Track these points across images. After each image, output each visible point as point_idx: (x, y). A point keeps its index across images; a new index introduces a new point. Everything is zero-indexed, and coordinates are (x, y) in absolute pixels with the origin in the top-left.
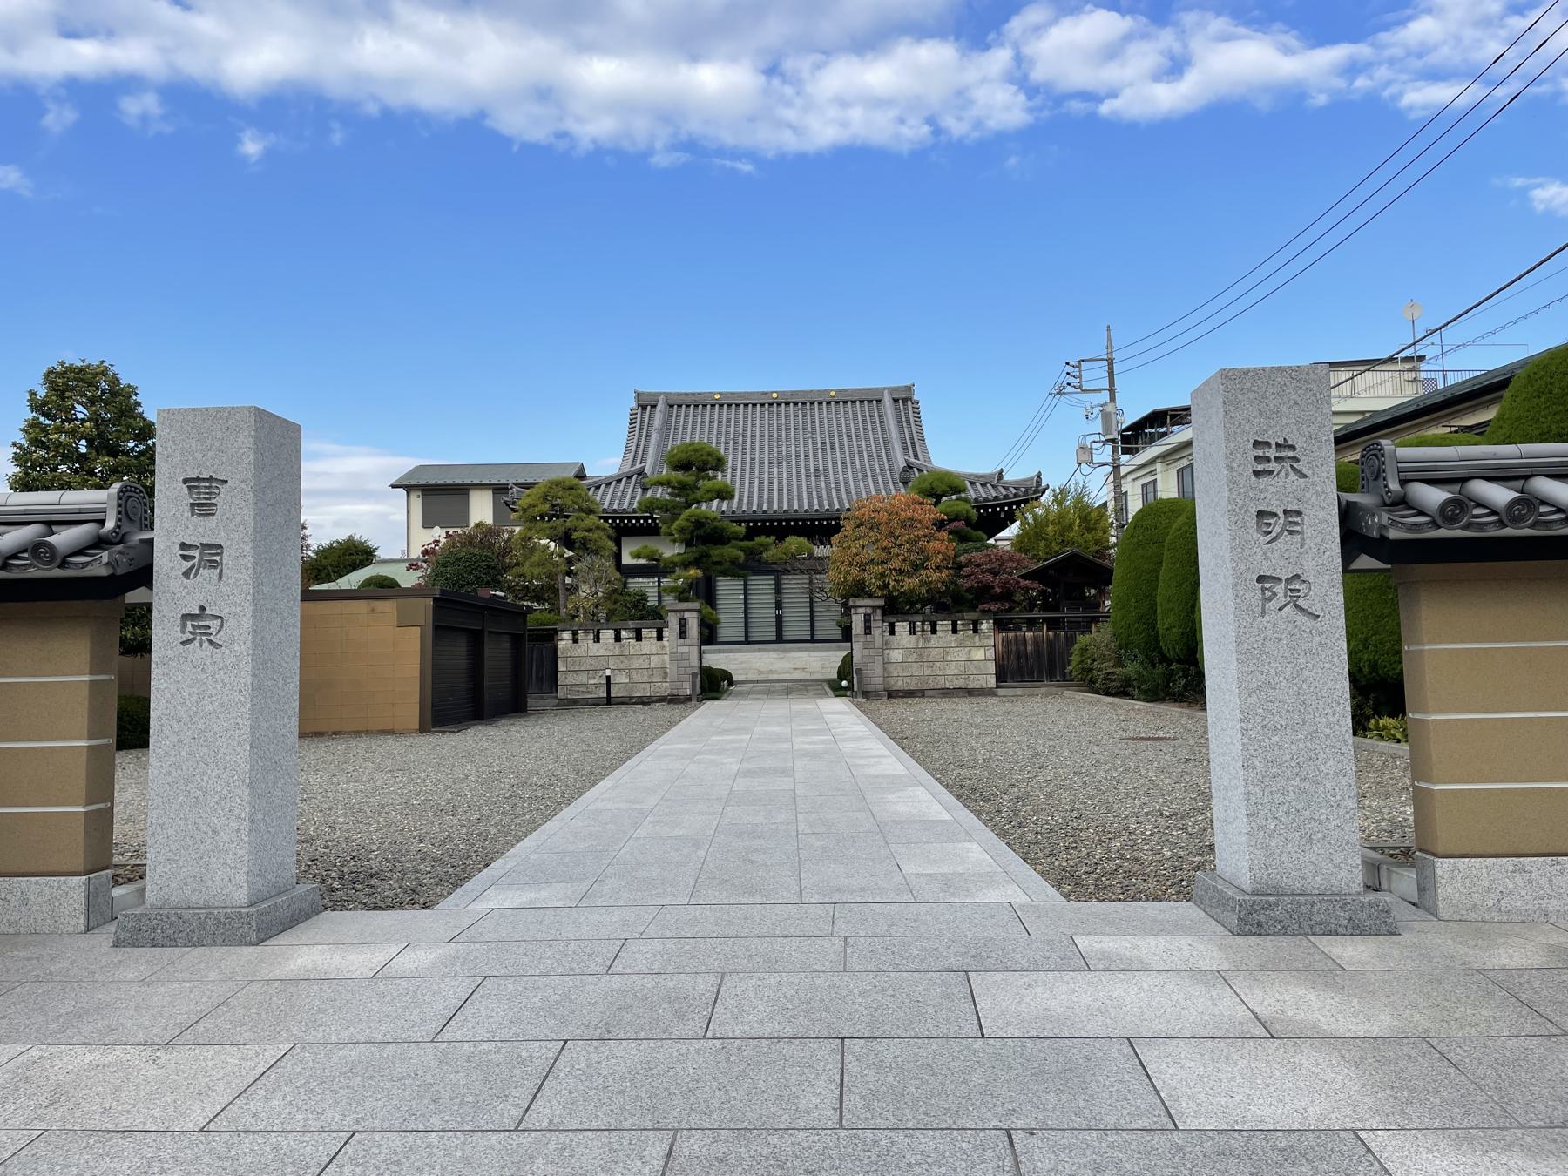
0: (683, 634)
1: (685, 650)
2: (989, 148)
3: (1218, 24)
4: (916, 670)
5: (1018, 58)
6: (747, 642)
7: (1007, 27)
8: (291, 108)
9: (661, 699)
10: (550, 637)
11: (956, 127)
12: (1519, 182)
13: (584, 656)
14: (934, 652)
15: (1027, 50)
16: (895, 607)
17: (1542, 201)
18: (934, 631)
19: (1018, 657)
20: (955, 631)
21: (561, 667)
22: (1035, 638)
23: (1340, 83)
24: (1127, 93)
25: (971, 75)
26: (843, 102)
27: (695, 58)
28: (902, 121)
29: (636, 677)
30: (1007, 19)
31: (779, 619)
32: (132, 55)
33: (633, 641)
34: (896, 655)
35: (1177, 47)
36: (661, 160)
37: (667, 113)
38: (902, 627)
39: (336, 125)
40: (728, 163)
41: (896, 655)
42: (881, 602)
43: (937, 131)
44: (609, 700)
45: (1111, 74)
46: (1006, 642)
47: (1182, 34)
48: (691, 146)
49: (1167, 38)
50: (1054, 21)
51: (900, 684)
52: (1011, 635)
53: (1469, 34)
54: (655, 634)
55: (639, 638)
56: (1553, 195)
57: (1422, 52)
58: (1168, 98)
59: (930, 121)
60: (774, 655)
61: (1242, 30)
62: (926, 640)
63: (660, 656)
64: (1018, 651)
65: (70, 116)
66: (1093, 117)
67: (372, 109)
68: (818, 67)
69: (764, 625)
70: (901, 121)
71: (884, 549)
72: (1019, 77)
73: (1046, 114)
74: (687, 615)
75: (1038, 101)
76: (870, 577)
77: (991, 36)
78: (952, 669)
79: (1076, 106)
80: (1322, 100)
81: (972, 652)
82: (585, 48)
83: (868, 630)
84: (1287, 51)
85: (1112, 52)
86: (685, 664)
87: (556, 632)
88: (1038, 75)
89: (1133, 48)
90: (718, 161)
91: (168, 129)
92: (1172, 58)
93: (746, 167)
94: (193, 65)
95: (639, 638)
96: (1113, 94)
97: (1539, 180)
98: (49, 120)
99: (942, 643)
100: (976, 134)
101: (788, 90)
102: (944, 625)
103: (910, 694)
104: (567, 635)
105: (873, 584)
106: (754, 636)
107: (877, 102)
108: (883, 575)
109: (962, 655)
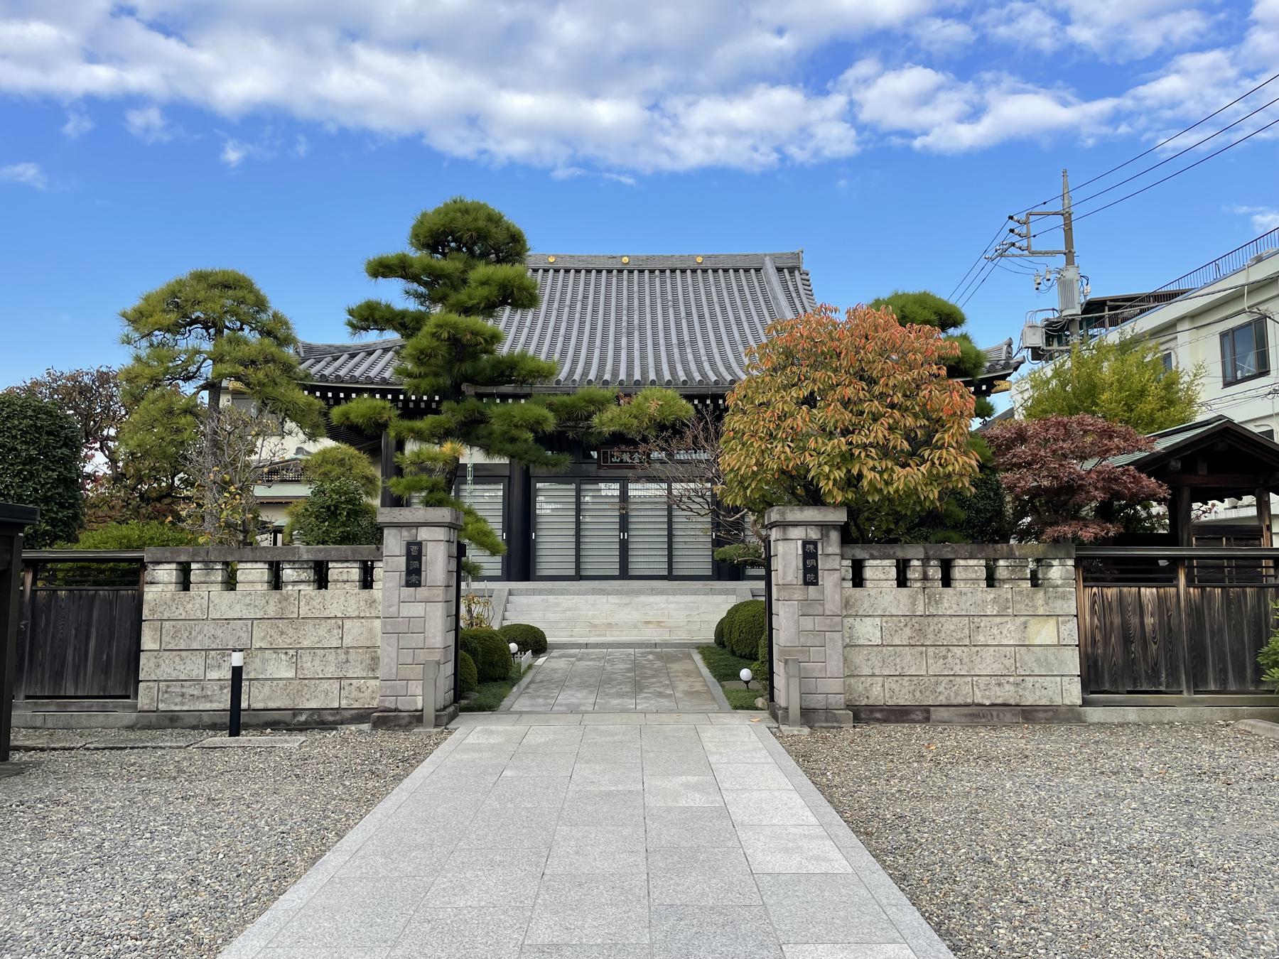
0: (413, 575)
1: (416, 610)
2: (828, 170)
3: (1009, 81)
4: (911, 663)
5: (852, 103)
6: (579, 577)
7: (842, 77)
8: (261, 122)
9: (361, 716)
10: (131, 575)
11: (798, 154)
12: (1244, 209)
13: (195, 624)
14: (949, 625)
15: (856, 96)
16: (875, 529)
17: (1261, 225)
18: (947, 581)
19: (1127, 640)
20: (991, 581)
21: (148, 641)
22: (1161, 600)
23: (1105, 130)
24: (936, 131)
25: (815, 115)
26: (710, 132)
27: (594, 95)
28: (755, 149)
29: (311, 666)
30: (842, 72)
31: (624, 547)
32: (140, 78)
33: (308, 589)
34: (868, 630)
35: (976, 99)
36: (561, 174)
37: (569, 137)
38: (880, 571)
39: (301, 138)
40: (615, 177)
41: (868, 630)
42: (841, 516)
43: (784, 157)
44: (235, 722)
45: (925, 116)
46: (1101, 608)
47: (981, 87)
48: (586, 164)
49: (968, 90)
50: (880, 75)
51: (878, 693)
52: (1111, 592)
53: (1210, 93)
54: (355, 573)
55: (322, 581)
56: (1268, 220)
57: (1174, 104)
58: (968, 135)
59: (778, 150)
60: (614, 599)
61: (1030, 86)
62: (932, 600)
63: (365, 628)
64: (1125, 626)
65: (87, 125)
66: (908, 150)
67: (332, 128)
68: (689, 105)
69: (602, 556)
70: (755, 149)
71: (846, 403)
72: (850, 115)
73: (871, 146)
74: (423, 534)
75: (867, 134)
76: (819, 463)
77: (830, 84)
78: (988, 663)
79: (896, 141)
80: (1091, 142)
81: (1023, 625)
82: (503, 85)
83: (810, 575)
84: (1065, 104)
85: (925, 99)
86: (416, 641)
87: (142, 565)
88: (865, 116)
89: (942, 97)
90: (607, 175)
91: (167, 138)
92: (974, 107)
93: (629, 181)
94: (188, 90)
95: (322, 581)
96: (925, 133)
97: (1261, 208)
98: (69, 128)
99: (966, 606)
100: (815, 161)
101: (667, 123)
102: (969, 569)
103: (898, 714)
104: (165, 574)
105: (830, 480)
106: (589, 568)
107: (736, 133)
108: (848, 457)
109: (1008, 633)
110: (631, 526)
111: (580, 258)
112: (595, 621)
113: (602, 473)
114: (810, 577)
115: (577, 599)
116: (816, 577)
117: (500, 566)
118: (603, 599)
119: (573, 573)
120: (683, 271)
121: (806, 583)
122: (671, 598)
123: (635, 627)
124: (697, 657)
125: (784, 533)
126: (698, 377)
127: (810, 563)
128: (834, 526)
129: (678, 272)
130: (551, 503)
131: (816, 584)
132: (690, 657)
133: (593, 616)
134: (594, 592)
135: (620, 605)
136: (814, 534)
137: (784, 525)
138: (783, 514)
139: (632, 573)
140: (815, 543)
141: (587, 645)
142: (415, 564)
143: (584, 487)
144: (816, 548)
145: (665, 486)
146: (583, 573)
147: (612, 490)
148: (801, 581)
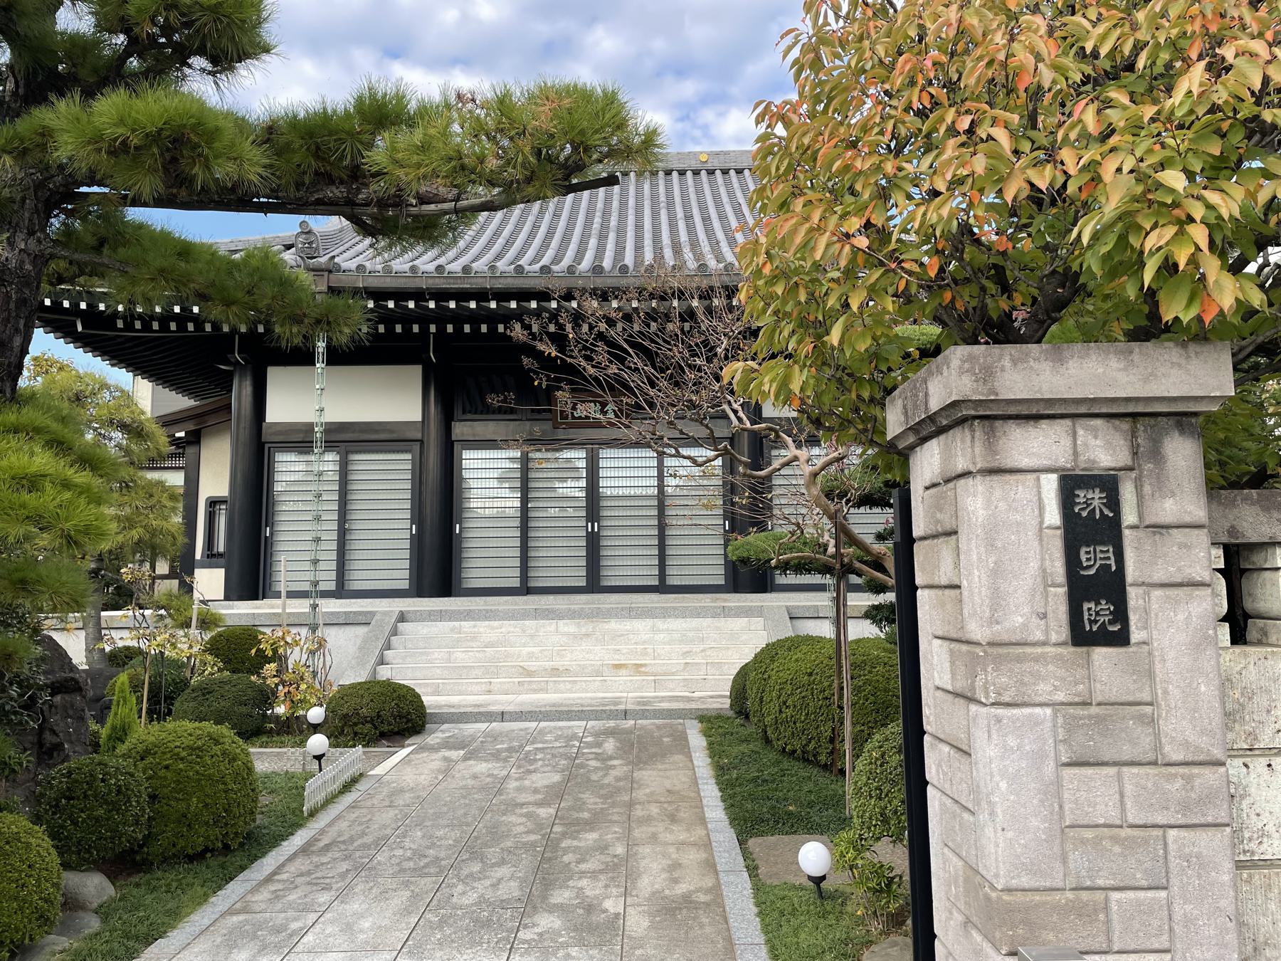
6: (526, 589)
31: (594, 544)
60: (568, 627)
69: (561, 557)
83: (1097, 604)
110: (604, 513)
112: (532, 665)
113: (561, 434)
114: (1097, 611)
115: (508, 626)
116: (1121, 614)
117: (406, 574)
118: (550, 626)
119: (516, 583)
120: (682, 173)
121: (1082, 636)
122: (660, 623)
123: (598, 673)
124: (697, 741)
125: (991, 444)
126: (692, 265)
127: (1093, 558)
128: (1182, 418)
129: (675, 174)
130: (487, 475)
131: (1121, 639)
132: (681, 743)
133: (531, 656)
134: (538, 614)
135: (575, 636)
136: (1102, 449)
137: (988, 416)
138: (987, 374)
139: (605, 583)
140: (1108, 484)
141: (502, 716)
142: (1093, 558)
144: (1113, 502)
146: (532, 584)
147: (578, 457)
148: (1059, 628)
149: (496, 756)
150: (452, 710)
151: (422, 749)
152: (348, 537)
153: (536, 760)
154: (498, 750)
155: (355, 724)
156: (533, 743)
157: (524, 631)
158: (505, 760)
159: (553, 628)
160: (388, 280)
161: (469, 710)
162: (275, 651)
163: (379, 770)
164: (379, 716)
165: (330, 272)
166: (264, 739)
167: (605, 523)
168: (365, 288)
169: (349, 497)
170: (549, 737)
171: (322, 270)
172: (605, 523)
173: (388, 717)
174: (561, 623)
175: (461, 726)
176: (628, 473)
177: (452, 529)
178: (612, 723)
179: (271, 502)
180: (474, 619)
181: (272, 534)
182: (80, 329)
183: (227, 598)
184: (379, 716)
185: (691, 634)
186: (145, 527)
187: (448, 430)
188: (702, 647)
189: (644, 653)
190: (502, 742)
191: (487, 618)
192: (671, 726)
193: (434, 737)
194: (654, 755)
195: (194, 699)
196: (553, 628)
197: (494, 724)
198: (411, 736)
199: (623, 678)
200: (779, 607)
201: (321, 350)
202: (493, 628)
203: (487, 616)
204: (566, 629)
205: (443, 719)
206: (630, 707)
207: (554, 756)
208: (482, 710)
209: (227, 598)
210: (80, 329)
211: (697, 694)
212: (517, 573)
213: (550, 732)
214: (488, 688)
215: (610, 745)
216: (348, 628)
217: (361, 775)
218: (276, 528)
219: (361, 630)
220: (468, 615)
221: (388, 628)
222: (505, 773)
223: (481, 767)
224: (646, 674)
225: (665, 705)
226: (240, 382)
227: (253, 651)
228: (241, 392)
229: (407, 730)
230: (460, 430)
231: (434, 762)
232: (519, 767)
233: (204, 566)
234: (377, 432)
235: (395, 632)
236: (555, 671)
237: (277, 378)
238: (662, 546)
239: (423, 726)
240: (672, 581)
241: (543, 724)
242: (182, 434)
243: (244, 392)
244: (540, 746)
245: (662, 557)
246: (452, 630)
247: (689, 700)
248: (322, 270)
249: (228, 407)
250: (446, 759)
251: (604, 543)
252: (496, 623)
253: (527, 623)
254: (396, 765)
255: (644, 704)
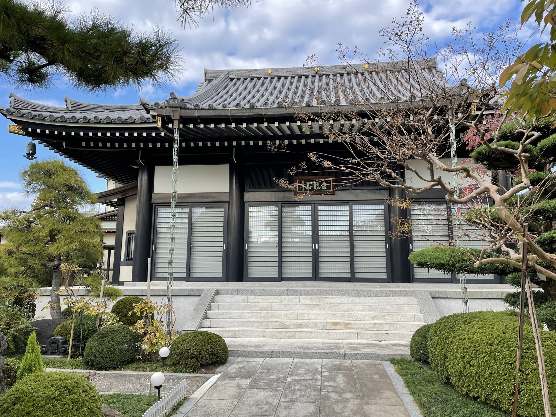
6: (281, 278)
60: (305, 300)
69: (299, 262)
106: (288, 272)
110: (321, 239)
111: (288, 70)
112: (286, 321)
117: (220, 270)
118: (295, 299)
119: (276, 275)
122: (357, 300)
124: (390, 369)
130: (260, 219)
133: (286, 316)
134: (289, 292)
139: (322, 276)
141: (272, 354)
143: (284, 209)
145: (347, 208)
146: (284, 276)
149: (269, 386)
150: (243, 349)
151: (225, 377)
152: (192, 251)
153: (295, 391)
154: (271, 380)
155: (187, 359)
156: (292, 375)
157: (281, 302)
158: (276, 389)
159: (297, 300)
160: (211, 111)
161: (252, 349)
162: (142, 313)
163: (197, 394)
164: (200, 354)
165: (181, 108)
166: (135, 365)
167: (321, 244)
168: (199, 116)
169: (193, 230)
170: (301, 371)
171: (177, 107)
172: (321, 244)
173: (205, 354)
174: (301, 297)
175: (248, 359)
176: (333, 220)
177: (243, 247)
178: (337, 362)
179: (155, 233)
180: (254, 294)
181: (155, 249)
182: (64, 147)
183: (133, 280)
184: (200, 354)
185: (375, 306)
186: (79, 242)
187: (241, 197)
188: (383, 314)
189: (349, 316)
190: (273, 374)
191: (261, 294)
192: (375, 365)
193: (232, 367)
194: (372, 391)
195: (97, 340)
196: (297, 300)
197: (267, 359)
198: (219, 365)
199: (339, 331)
200: (425, 292)
201: (176, 149)
202: (265, 299)
203: (262, 292)
204: (304, 301)
205: (238, 354)
206: (348, 351)
207: (306, 387)
208: (260, 349)
209: (133, 280)
210: (64, 147)
211: (383, 343)
212: (276, 270)
213: (301, 367)
214: (263, 334)
215: (340, 380)
216: (189, 298)
217: (185, 398)
218: (157, 246)
219: (196, 299)
220: (252, 292)
221: (209, 299)
222: (276, 401)
223: (261, 395)
224: (351, 329)
225: (368, 351)
226: (142, 175)
227: (130, 313)
228: (143, 179)
229: (217, 362)
230: (248, 196)
231: (230, 388)
232: (286, 396)
233: (125, 264)
234: (207, 197)
235: (213, 301)
236: (300, 326)
237: (160, 172)
238: (352, 257)
239: (226, 359)
240: (357, 276)
241: (296, 360)
242: (116, 200)
243: (144, 179)
244: (296, 378)
245: (352, 262)
246: (243, 300)
247: (381, 347)
248: (177, 107)
249: (136, 187)
250: (239, 387)
251: (321, 255)
252: (267, 297)
253: (283, 297)
254: (209, 387)
255: (355, 349)
